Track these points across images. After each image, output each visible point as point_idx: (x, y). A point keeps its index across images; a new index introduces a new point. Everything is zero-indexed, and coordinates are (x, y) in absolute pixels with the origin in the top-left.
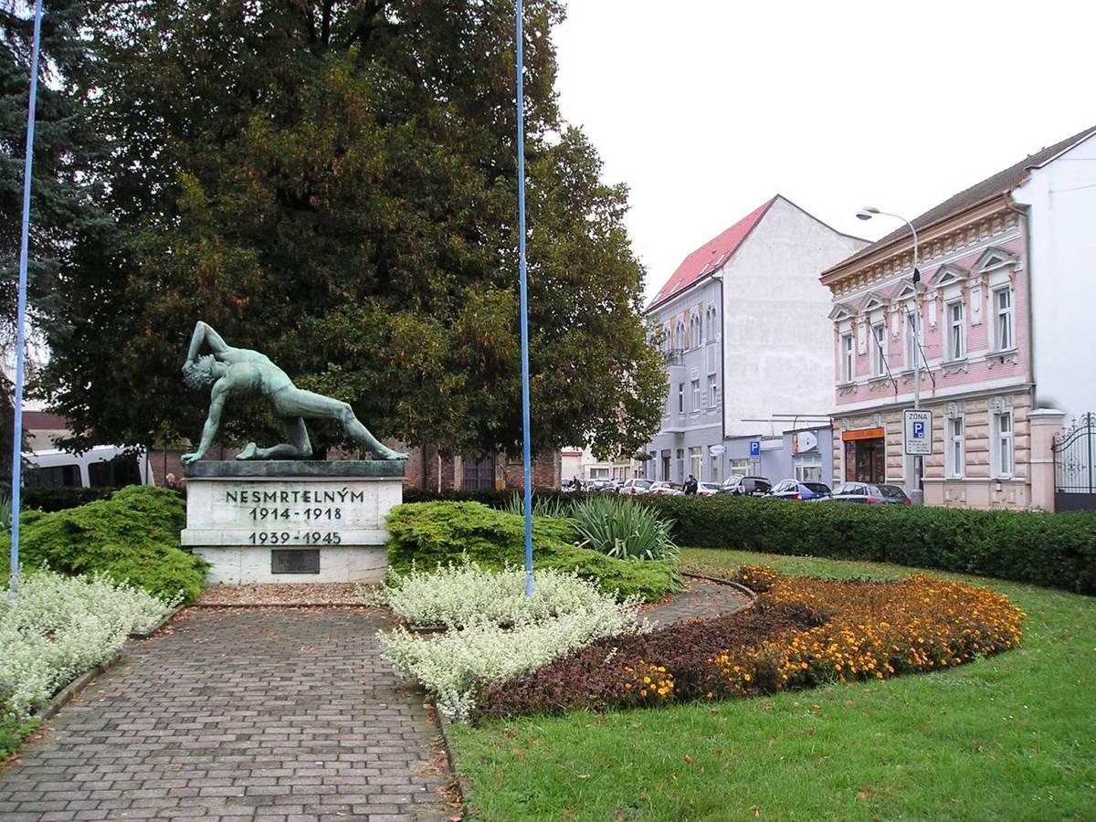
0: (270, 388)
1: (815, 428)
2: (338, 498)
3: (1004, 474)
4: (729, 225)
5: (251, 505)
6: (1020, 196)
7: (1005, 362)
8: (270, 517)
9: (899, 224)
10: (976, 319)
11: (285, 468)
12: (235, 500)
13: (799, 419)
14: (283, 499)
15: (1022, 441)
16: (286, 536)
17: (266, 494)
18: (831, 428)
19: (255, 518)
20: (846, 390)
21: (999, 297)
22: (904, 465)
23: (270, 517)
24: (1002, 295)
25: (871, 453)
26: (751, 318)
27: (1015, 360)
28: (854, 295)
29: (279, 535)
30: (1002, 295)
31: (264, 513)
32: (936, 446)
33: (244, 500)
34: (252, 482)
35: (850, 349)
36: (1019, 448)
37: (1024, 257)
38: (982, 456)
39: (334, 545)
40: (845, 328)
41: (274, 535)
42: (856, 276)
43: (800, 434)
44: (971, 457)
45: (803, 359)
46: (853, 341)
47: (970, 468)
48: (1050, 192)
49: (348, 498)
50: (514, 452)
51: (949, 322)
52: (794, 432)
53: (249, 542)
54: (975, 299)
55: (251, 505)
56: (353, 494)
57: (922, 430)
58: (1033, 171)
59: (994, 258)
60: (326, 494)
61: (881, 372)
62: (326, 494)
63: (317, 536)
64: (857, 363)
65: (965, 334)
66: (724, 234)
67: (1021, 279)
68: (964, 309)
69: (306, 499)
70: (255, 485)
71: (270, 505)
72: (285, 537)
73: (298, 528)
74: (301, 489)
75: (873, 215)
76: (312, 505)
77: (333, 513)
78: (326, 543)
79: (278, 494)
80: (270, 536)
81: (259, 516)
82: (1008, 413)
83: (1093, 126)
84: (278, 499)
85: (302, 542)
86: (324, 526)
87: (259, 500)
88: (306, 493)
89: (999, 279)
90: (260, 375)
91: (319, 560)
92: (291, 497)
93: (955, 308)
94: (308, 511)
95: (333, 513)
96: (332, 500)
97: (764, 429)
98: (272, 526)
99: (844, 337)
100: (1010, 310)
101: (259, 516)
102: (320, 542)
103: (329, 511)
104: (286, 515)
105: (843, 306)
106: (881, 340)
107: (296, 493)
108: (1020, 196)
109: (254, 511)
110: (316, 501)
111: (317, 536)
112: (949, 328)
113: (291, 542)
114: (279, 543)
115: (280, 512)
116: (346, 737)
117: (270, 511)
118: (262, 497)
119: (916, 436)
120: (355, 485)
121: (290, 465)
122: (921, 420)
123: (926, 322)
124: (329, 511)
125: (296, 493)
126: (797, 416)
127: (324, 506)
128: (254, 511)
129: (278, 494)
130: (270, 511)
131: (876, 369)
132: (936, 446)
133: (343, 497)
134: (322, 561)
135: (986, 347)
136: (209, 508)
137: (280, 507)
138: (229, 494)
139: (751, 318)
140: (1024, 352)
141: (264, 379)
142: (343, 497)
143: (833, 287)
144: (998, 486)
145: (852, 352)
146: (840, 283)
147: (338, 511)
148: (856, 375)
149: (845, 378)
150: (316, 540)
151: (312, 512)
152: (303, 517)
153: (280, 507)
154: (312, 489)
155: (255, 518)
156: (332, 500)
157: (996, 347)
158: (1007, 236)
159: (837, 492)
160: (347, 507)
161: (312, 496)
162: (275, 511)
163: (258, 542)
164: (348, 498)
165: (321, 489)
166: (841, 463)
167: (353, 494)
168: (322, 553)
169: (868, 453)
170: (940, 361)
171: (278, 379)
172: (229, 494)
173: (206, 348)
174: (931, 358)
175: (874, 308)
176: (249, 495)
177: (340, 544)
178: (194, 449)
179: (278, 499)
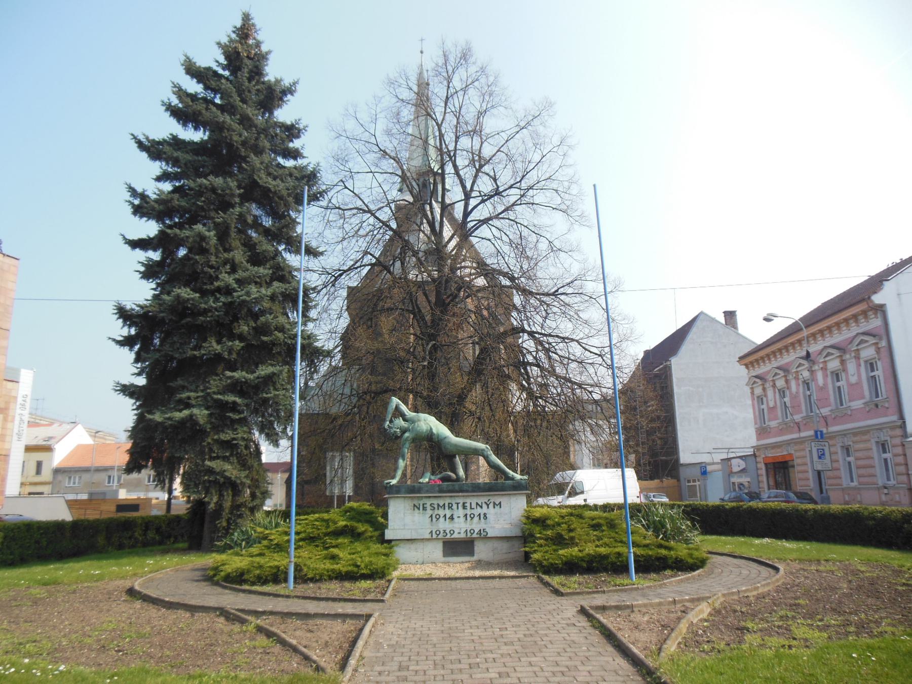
0: (438, 437)
1: (744, 456)
2: (485, 506)
3: (852, 484)
4: (839, 294)
5: (429, 512)
6: (877, 299)
7: (879, 407)
8: (442, 519)
9: (790, 322)
10: (853, 380)
11: (451, 488)
12: (419, 509)
13: (731, 450)
14: (449, 508)
15: (900, 459)
16: (452, 532)
17: (438, 505)
18: (754, 455)
19: (432, 520)
20: (762, 432)
21: (869, 366)
22: (878, 475)
23: (442, 519)
24: (872, 366)
25: (784, 472)
26: (691, 389)
27: (887, 405)
28: (762, 369)
29: (448, 532)
30: (872, 366)
31: (438, 517)
32: (835, 465)
33: (424, 509)
34: (430, 497)
35: (762, 404)
36: (897, 465)
37: (885, 337)
38: (870, 471)
39: (484, 537)
40: (758, 391)
41: (445, 531)
42: (762, 358)
43: (733, 461)
44: (862, 471)
45: (727, 413)
46: (765, 399)
47: (862, 479)
48: (899, 294)
49: (491, 506)
50: (349, 496)
51: (833, 383)
52: (729, 459)
53: (429, 536)
54: (851, 367)
55: (429, 512)
56: (494, 503)
57: (823, 454)
58: (885, 283)
59: (862, 340)
60: (477, 504)
61: (787, 418)
62: (477, 504)
63: (438, 533)
64: (769, 413)
65: (846, 390)
66: (838, 296)
67: (884, 353)
68: (843, 375)
69: (464, 507)
70: (431, 499)
71: (441, 512)
72: (452, 532)
73: (460, 528)
74: (461, 501)
75: (773, 318)
76: (469, 512)
77: (482, 516)
78: (478, 536)
79: (447, 505)
80: (442, 532)
81: (434, 519)
82: (887, 441)
83: (905, 257)
84: (447, 508)
85: (463, 535)
86: (476, 526)
87: (434, 508)
88: (464, 503)
89: (868, 353)
90: (431, 429)
91: (473, 548)
92: (455, 506)
93: (837, 376)
94: (466, 515)
95: (482, 516)
96: (481, 507)
97: (705, 458)
98: (443, 525)
99: (758, 397)
100: (879, 373)
101: (434, 519)
102: (475, 535)
103: (480, 515)
104: (452, 518)
105: (756, 377)
106: (784, 397)
107: (458, 504)
108: (877, 299)
109: (431, 516)
110: (471, 508)
111: (472, 531)
112: (868, 379)
113: (455, 536)
114: (448, 536)
115: (448, 516)
116: (475, 670)
117: (442, 516)
118: (436, 506)
119: (820, 458)
120: (496, 497)
121: (453, 485)
122: (821, 447)
123: (817, 384)
124: (480, 515)
125: (458, 504)
126: (729, 449)
127: (478, 511)
128: (431, 516)
129: (447, 505)
130: (442, 516)
131: (782, 416)
132: (835, 465)
133: (488, 506)
134: (476, 548)
135: (863, 397)
136: (402, 515)
137: (448, 513)
138: (415, 505)
139: (691, 389)
140: (893, 400)
141: (435, 431)
142: (488, 506)
143: (747, 366)
144: (886, 491)
145: (764, 406)
146: (752, 363)
147: (485, 515)
148: (769, 421)
149: (761, 423)
150: (472, 534)
151: (468, 516)
152: (462, 519)
153: (448, 513)
154: (468, 501)
155: (432, 520)
156: (481, 507)
157: (871, 397)
158: (875, 323)
159: (765, 496)
160: (491, 512)
161: (468, 505)
162: (445, 516)
163: (434, 536)
164: (491, 506)
165: (474, 501)
166: (764, 479)
167: (494, 503)
168: (476, 543)
169: (782, 471)
170: (829, 408)
171: (441, 429)
172: (415, 505)
173: (398, 413)
174: (822, 407)
175: (778, 377)
176: (428, 506)
177: (489, 536)
178: (393, 478)
179: (447, 508)
